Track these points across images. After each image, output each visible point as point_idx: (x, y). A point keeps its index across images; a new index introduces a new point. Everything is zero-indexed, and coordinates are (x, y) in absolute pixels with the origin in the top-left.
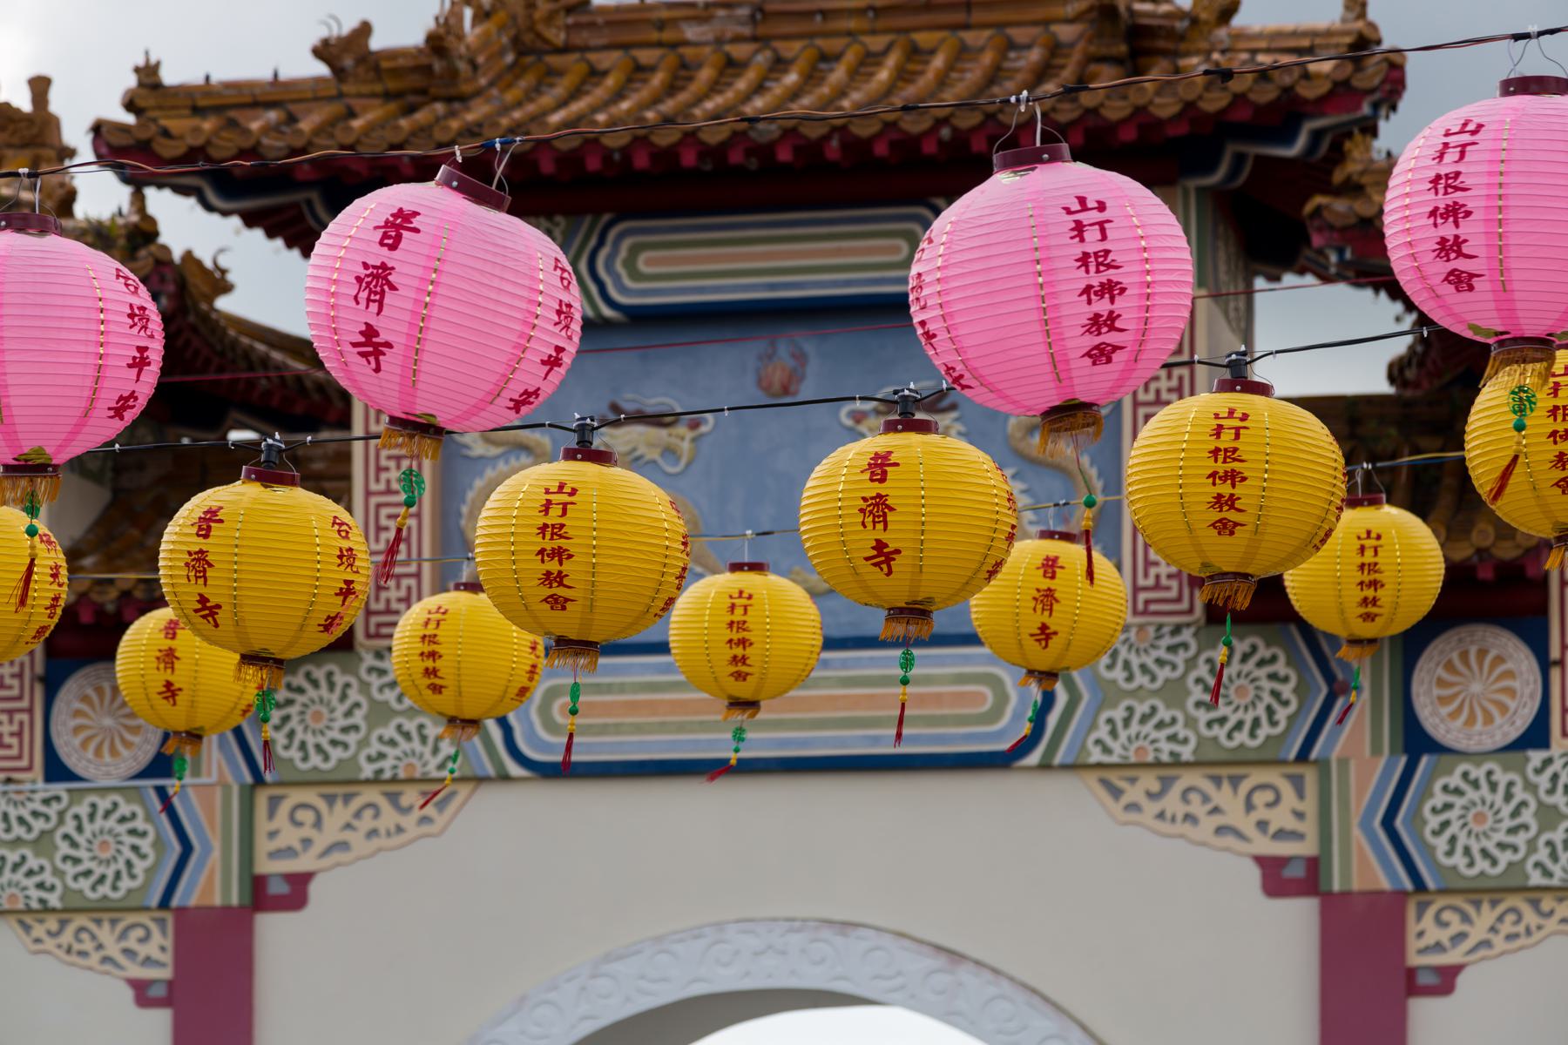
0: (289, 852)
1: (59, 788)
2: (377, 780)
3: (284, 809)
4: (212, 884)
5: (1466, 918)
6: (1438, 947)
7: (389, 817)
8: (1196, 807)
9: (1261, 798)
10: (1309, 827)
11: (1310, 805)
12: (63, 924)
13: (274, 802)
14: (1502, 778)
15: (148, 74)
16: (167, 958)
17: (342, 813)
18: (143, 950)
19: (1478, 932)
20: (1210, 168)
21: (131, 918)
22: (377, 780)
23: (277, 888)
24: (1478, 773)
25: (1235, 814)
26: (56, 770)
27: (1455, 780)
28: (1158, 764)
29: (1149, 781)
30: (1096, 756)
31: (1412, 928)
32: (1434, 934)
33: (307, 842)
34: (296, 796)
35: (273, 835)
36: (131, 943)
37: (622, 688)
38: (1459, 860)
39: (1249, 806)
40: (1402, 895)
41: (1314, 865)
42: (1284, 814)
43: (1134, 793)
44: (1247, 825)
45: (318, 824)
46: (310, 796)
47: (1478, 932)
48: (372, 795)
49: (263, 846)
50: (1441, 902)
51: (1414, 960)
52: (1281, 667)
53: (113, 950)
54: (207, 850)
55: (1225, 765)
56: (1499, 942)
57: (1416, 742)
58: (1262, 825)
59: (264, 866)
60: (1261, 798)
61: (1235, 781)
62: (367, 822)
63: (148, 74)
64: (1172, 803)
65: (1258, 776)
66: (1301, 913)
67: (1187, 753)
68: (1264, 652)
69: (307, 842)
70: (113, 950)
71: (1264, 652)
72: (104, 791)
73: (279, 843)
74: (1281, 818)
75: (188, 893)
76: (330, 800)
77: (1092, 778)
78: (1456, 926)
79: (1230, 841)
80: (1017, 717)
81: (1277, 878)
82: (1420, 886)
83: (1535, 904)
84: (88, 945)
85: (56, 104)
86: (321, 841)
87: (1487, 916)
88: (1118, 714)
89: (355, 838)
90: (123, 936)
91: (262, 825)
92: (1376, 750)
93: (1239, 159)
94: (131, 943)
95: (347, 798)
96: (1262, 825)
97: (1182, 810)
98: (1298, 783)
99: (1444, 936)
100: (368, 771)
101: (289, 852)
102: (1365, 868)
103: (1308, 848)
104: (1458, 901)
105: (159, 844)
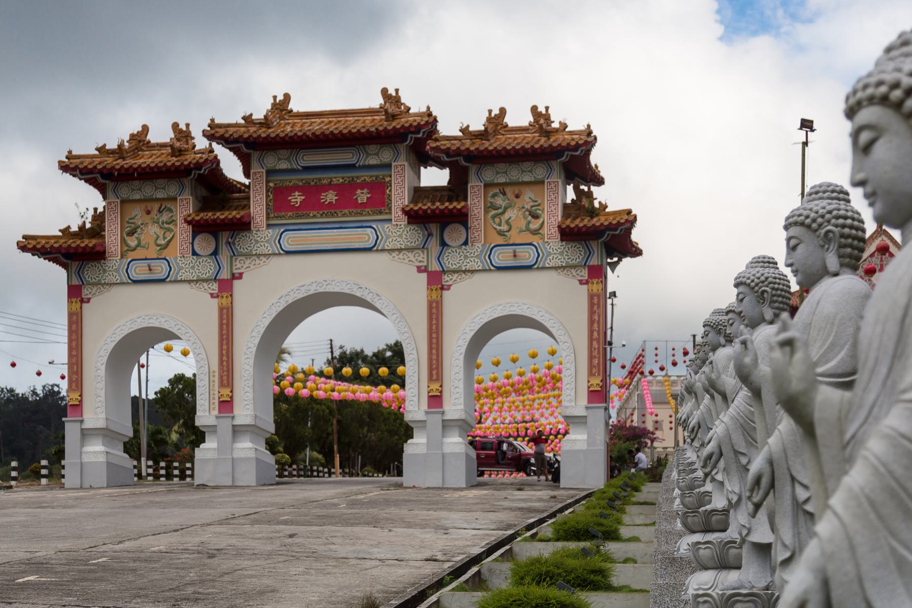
7: (258, 261)
8: (405, 257)
10: (425, 260)
11: (425, 256)
23: (237, 275)
26: (194, 253)
34: (240, 258)
49: (234, 267)
55: (410, 249)
66: (425, 275)
81: (420, 270)
87: (95, 289)
103: (425, 264)
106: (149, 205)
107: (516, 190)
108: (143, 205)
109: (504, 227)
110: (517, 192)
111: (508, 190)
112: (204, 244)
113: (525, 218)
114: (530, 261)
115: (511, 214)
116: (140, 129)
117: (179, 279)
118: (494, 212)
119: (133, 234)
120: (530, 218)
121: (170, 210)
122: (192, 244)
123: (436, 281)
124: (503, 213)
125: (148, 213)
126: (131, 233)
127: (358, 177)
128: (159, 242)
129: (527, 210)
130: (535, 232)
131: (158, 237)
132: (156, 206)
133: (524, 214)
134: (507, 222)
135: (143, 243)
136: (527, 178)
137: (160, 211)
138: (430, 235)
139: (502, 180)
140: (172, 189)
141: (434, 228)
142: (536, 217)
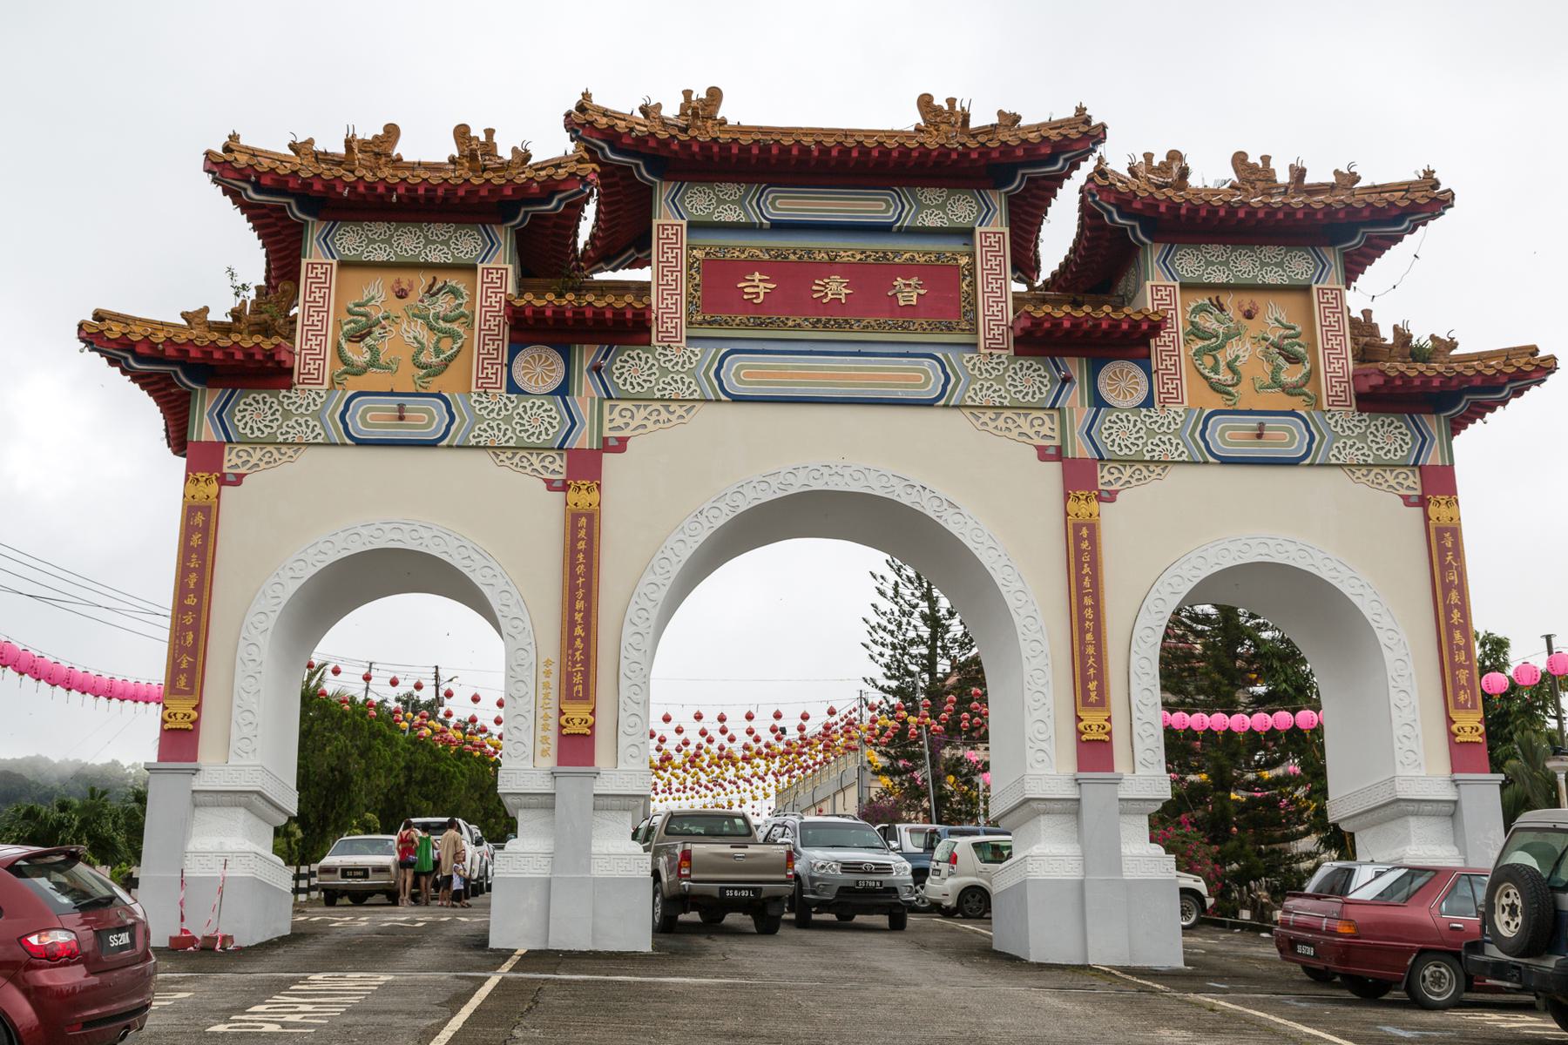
0: (619, 428)
1: (513, 397)
2: (662, 399)
3: (617, 410)
4: (583, 439)
5: (249, 455)
6: (237, 466)
7: (664, 415)
9: (1036, 422)
10: (1056, 434)
11: (1056, 426)
12: (515, 454)
13: (612, 408)
14: (1132, 419)
15: (234, 137)
16: (563, 470)
17: (643, 413)
18: (1406, 483)
19: (1125, 478)
20: (514, 218)
21: (546, 453)
22: (662, 399)
24: (1122, 416)
25: (1026, 428)
26: (513, 388)
27: (1113, 418)
28: (995, 407)
29: (991, 413)
30: (969, 402)
31: (226, 457)
32: (1108, 477)
33: (627, 424)
34: (623, 405)
35: (611, 421)
36: (546, 463)
37: (822, 368)
38: (1116, 448)
39: (1032, 426)
40: (221, 445)
41: (1059, 449)
42: (1045, 428)
43: (985, 418)
44: (1031, 432)
45: (632, 417)
46: (628, 405)
47: (1125, 478)
48: (657, 405)
49: (606, 425)
50: (240, 447)
51: (225, 470)
52: (1042, 372)
53: (537, 466)
54: (583, 423)
56: (262, 465)
57: (1098, 402)
58: (1037, 433)
59: (606, 433)
60: (1036, 422)
61: (1026, 415)
62: (654, 417)
63: (234, 137)
64: (1000, 422)
65: (1036, 414)
66: (1055, 468)
67: (1006, 403)
68: (1035, 366)
69: (627, 424)
70: (537, 466)
71: (1035, 366)
72: (1122, 411)
73: (615, 424)
74: (1045, 430)
75: (574, 440)
76: (638, 407)
77: (967, 412)
78: (245, 457)
79: (1024, 438)
80: (935, 385)
82: (230, 441)
83: (279, 450)
84: (526, 464)
85: (496, 138)
86: (633, 424)
87: (1128, 471)
88: (978, 387)
89: (649, 424)
90: (543, 460)
91: (606, 416)
92: (1083, 405)
93: (526, 213)
94: (546, 463)
95: (646, 407)
96: (1037, 433)
97: (1004, 426)
98: (1051, 417)
99: (1111, 478)
100: (658, 395)
101: (619, 428)
102: (1080, 449)
103: (1056, 442)
104: (246, 447)
105: (562, 421)
106: (405, 278)
107: (1246, 300)
108: (391, 277)
109: (1225, 376)
110: (1247, 307)
111: (1229, 300)
112: (539, 369)
113: (1271, 361)
114: (1296, 449)
115: (1241, 350)
116: (381, 132)
117: (473, 442)
118: (1201, 344)
119: (362, 338)
120: (1281, 360)
121: (455, 293)
122: (509, 366)
123: (1080, 478)
124: (1222, 346)
125: (402, 295)
126: (358, 337)
127: (896, 253)
128: (423, 359)
129: (1272, 344)
130: (1292, 391)
131: (422, 348)
132: (422, 280)
133: (1266, 354)
134: (1231, 366)
135: (383, 360)
136: (1272, 278)
137: (431, 292)
138: (1067, 380)
139: (1220, 277)
140: (465, 245)
141: (1075, 367)
142: (1294, 359)
